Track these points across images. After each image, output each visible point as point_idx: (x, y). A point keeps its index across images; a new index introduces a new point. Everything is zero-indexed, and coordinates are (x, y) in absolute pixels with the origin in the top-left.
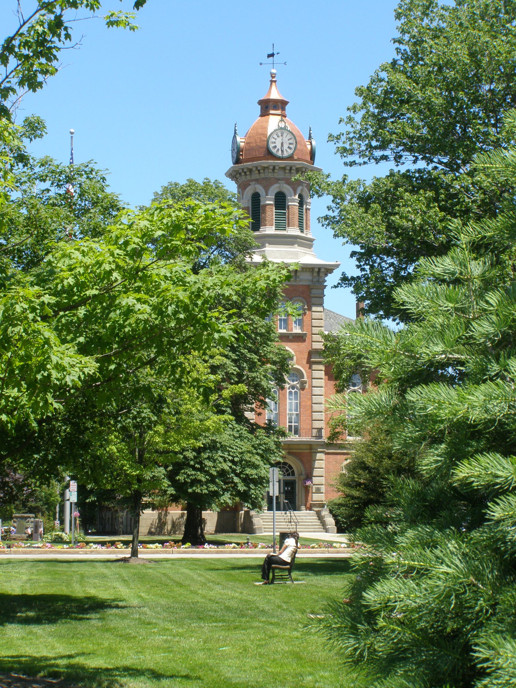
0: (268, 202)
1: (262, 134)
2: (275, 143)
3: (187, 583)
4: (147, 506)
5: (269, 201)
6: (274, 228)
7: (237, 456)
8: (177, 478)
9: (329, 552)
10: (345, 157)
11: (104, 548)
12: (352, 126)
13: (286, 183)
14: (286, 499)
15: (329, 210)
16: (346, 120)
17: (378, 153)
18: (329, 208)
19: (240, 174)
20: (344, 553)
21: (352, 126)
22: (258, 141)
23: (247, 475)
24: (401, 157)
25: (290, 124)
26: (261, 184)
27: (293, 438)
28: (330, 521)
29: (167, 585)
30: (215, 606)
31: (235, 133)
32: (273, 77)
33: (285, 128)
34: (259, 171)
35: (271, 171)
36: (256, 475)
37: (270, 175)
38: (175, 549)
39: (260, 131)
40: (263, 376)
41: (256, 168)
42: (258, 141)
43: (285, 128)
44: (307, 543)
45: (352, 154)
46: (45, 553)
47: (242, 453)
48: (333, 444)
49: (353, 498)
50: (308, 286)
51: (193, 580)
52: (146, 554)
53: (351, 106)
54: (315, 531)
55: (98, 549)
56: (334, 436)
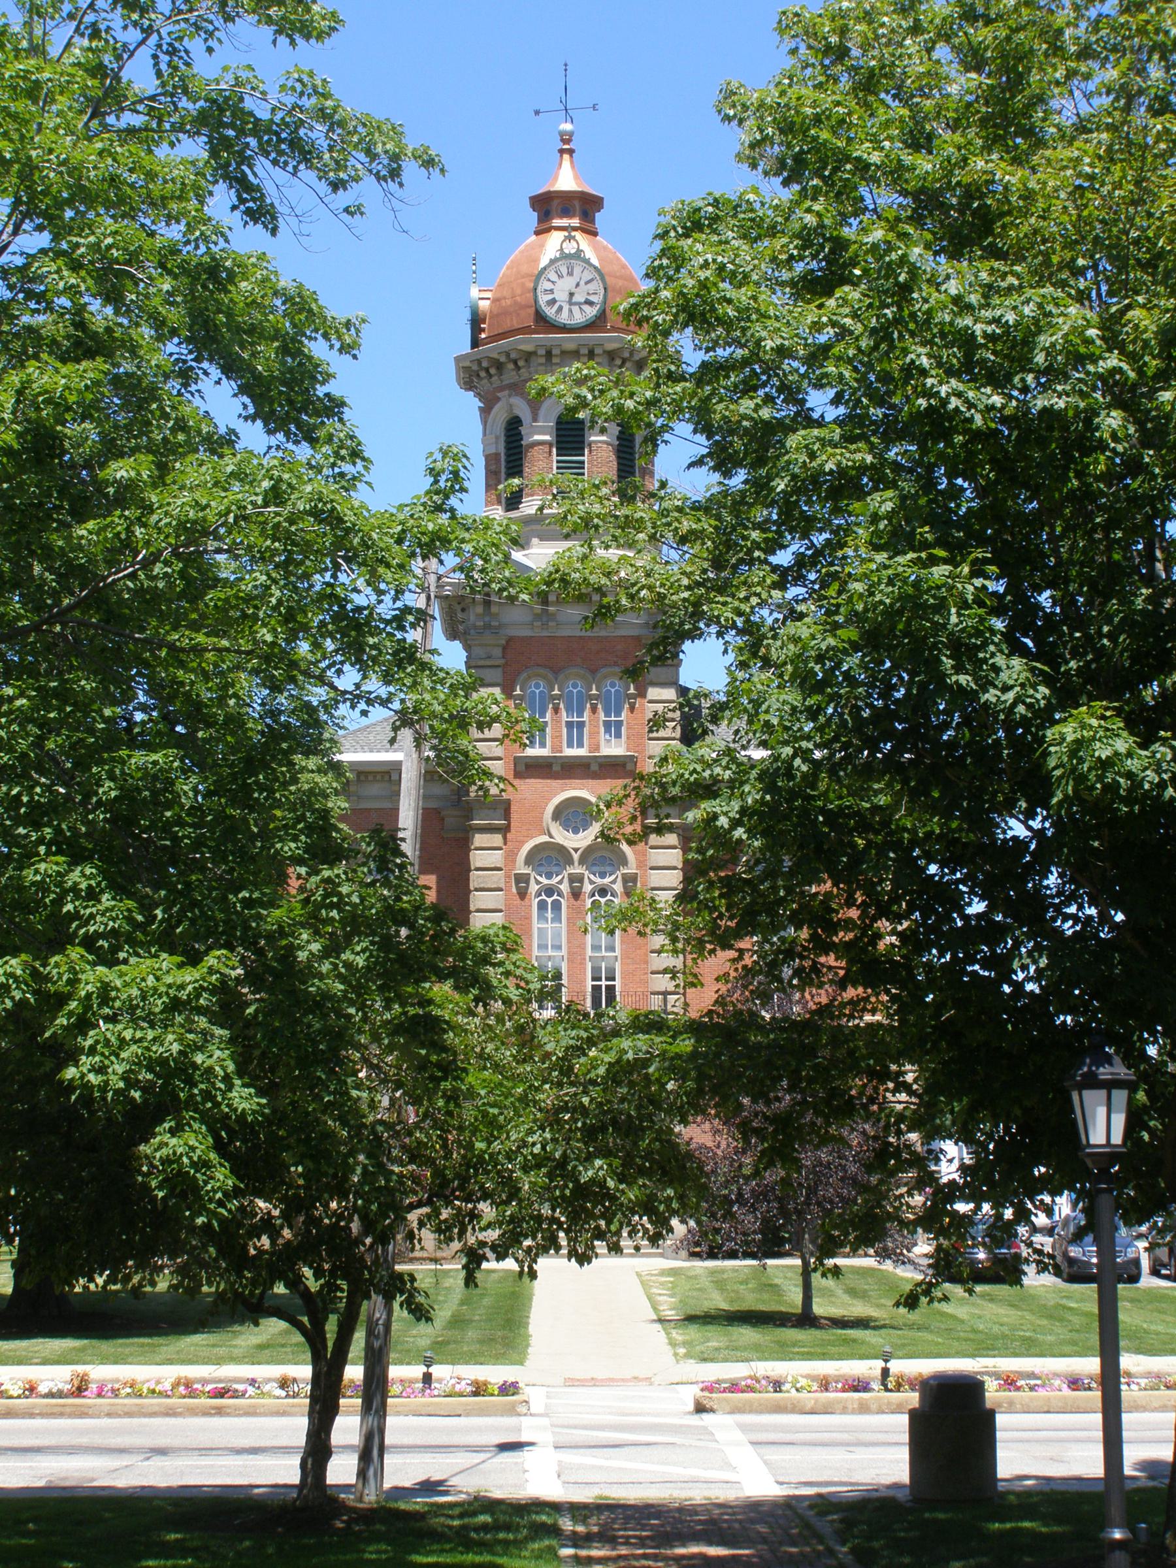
0: (537, 437)
5: (540, 434)
20: (32, 1415)
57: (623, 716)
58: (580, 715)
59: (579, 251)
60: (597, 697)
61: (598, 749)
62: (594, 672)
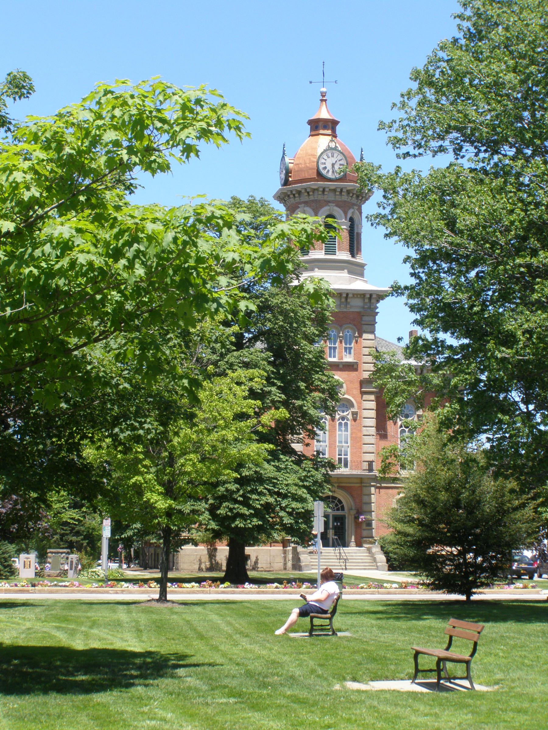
1: (312, 155)
2: (325, 163)
3: (211, 634)
4: (186, 541)
6: (324, 253)
7: (283, 489)
8: (218, 512)
9: (379, 593)
10: (397, 148)
11: (136, 588)
12: (406, 112)
13: (337, 206)
14: (335, 535)
15: (379, 207)
16: (399, 105)
17: (435, 144)
18: (379, 205)
19: (289, 196)
20: (396, 594)
21: (406, 112)
22: (308, 162)
23: (293, 509)
24: (461, 148)
25: (341, 144)
26: (310, 207)
27: (342, 471)
28: (381, 558)
29: (186, 637)
30: (234, 669)
31: (284, 154)
32: (323, 96)
33: (335, 148)
34: (308, 193)
35: (320, 193)
36: (303, 508)
37: (320, 197)
38: (213, 589)
39: (309, 151)
40: (309, 404)
41: (306, 189)
42: (308, 162)
43: (335, 148)
44: (357, 582)
45: (406, 144)
46: (73, 592)
47: (287, 485)
48: (386, 480)
49: (406, 535)
50: (359, 313)
51: (218, 629)
52: (175, 594)
53: (405, 91)
54: (365, 569)
55: (129, 588)
56: (385, 469)
57: (352, 345)
58: (335, 344)
59: (336, 147)
60: (342, 337)
61: (342, 359)
62: (341, 326)
